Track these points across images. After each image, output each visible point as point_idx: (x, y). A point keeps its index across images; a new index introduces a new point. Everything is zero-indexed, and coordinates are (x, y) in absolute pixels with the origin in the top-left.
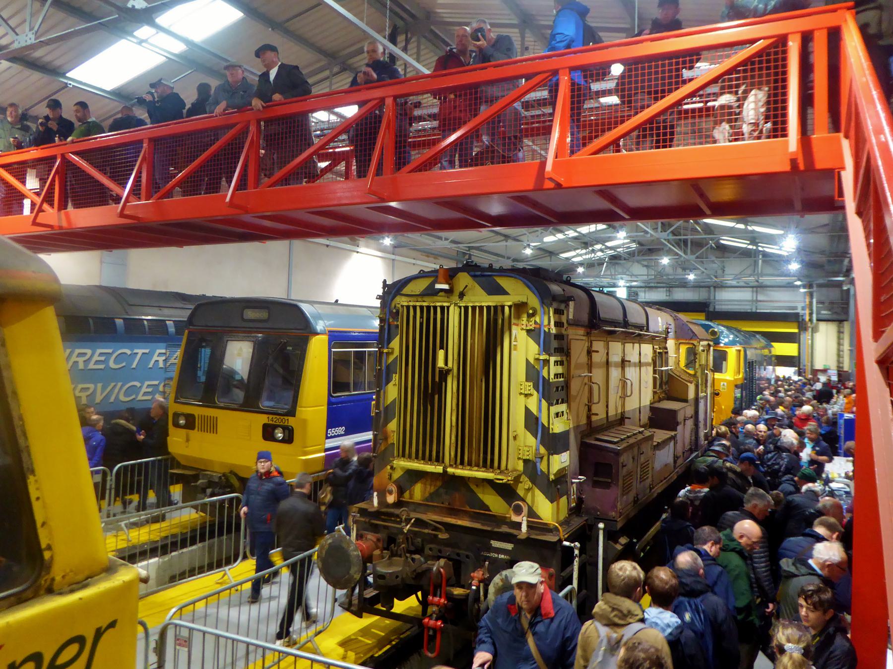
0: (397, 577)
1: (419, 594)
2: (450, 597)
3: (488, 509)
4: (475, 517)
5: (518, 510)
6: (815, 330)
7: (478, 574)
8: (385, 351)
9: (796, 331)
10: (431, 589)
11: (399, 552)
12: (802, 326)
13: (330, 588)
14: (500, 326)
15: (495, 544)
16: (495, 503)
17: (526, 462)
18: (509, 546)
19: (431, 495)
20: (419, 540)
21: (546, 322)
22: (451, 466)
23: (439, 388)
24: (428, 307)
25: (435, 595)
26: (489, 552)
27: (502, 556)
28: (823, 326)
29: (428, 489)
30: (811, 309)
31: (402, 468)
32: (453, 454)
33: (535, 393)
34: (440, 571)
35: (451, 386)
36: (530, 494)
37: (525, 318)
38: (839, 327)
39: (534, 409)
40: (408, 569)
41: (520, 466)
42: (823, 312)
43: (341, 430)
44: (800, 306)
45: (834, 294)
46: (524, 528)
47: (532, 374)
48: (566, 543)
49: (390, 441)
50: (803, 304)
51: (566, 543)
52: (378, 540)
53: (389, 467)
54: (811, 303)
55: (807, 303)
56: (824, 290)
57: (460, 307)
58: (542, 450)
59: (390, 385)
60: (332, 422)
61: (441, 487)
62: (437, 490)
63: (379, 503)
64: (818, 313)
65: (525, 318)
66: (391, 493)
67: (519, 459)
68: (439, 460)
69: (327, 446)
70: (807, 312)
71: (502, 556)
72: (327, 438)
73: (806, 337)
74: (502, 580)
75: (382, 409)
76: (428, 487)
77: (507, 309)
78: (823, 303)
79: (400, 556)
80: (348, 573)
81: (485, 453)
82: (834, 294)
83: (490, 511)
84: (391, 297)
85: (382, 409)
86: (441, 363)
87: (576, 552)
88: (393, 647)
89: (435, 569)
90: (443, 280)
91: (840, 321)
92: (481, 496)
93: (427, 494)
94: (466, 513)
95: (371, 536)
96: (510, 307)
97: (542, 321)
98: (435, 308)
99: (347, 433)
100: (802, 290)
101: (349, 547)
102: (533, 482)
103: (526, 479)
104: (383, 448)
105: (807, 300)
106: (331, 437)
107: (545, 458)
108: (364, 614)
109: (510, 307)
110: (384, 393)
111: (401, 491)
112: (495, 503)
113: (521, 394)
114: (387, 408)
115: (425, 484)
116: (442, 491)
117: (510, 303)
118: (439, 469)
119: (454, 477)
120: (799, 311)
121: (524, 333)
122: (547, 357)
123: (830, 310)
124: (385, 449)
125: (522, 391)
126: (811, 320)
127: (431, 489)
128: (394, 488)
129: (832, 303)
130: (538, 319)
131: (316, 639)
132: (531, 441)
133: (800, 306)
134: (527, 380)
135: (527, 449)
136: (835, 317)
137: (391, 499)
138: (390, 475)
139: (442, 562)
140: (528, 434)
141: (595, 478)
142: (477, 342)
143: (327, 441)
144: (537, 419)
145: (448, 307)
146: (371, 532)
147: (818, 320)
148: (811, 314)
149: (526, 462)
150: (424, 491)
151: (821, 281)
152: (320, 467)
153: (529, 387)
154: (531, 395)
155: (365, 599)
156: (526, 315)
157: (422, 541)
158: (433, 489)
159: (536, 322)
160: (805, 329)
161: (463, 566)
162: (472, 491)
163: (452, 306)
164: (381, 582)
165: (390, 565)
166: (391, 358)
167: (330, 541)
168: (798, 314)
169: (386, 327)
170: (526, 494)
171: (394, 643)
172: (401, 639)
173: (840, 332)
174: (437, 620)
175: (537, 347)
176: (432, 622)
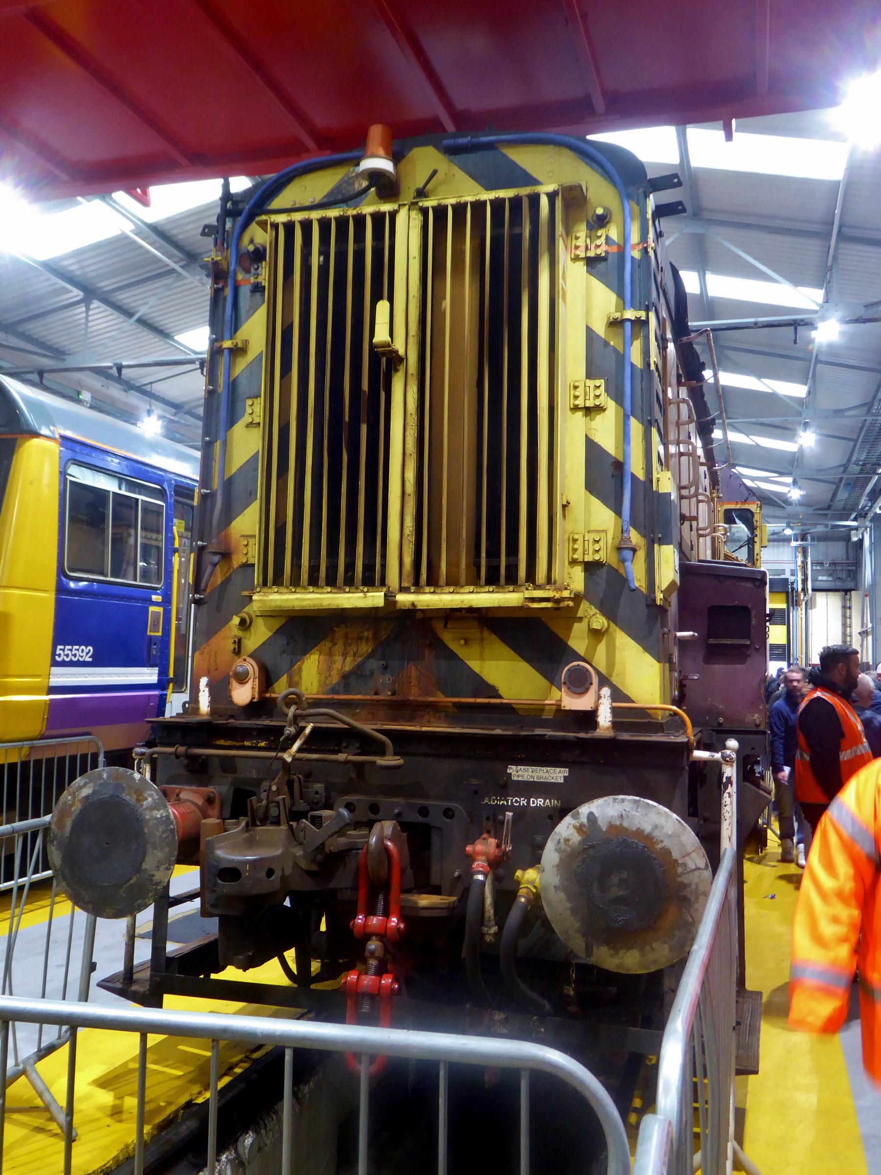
0: (270, 873)
1: (290, 955)
2: (409, 916)
3: (493, 692)
4: (464, 712)
5: (579, 683)
6: (810, 605)
7: (485, 847)
8: (227, 344)
9: (784, 606)
10: (362, 896)
11: (274, 812)
12: (792, 598)
13: (82, 916)
14: (526, 244)
15: (520, 773)
16: (509, 676)
17: (591, 568)
18: (557, 775)
19: (345, 677)
20: (319, 787)
21: (635, 237)
22: (403, 590)
23: (374, 408)
24: (342, 222)
25: (370, 911)
26: (505, 796)
27: (540, 802)
28: (821, 598)
29: (338, 665)
30: (805, 574)
31: (271, 614)
32: (408, 560)
33: (611, 405)
34: (386, 849)
35: (402, 397)
36: (602, 648)
37: (581, 231)
38: (844, 600)
39: (608, 443)
40: (299, 852)
41: (577, 580)
42: (820, 578)
43: (85, 652)
44: (788, 568)
45: (837, 551)
46: (605, 718)
47: (601, 360)
48: (700, 754)
49: (238, 560)
50: (793, 566)
51: (700, 754)
52: (210, 801)
53: (236, 620)
54: (804, 563)
55: (799, 563)
56: (822, 545)
57: (424, 212)
58: (635, 537)
59: (239, 428)
60: (65, 633)
61: (370, 656)
62: (360, 666)
63: (212, 703)
64: (814, 580)
65: (581, 231)
66: (242, 679)
67: (573, 562)
68: (372, 578)
69: (55, 681)
70: (800, 577)
71: (540, 802)
72: (55, 664)
73: (797, 615)
74: (580, 829)
75: (216, 484)
76: (338, 659)
77: (544, 201)
78: (821, 564)
79: (277, 822)
80: (139, 870)
81: (493, 553)
82: (837, 551)
83: (500, 697)
84: (240, 220)
85: (216, 484)
86: (381, 335)
87: (730, 771)
88: (238, 1079)
89: (373, 840)
90: (381, 152)
91: (847, 591)
92: (475, 665)
93: (335, 679)
94: (434, 708)
95: (191, 795)
96: (552, 196)
97: (625, 236)
98: (360, 220)
99: (98, 661)
100: (794, 544)
101: (140, 799)
102: (611, 615)
103: (593, 610)
104: (219, 579)
105: (800, 559)
106: (63, 664)
107: (641, 555)
108: (167, 998)
109: (552, 196)
110: (225, 444)
111: (267, 679)
112: (509, 676)
113: (575, 408)
114: (228, 484)
115: (330, 654)
116: (374, 664)
117: (550, 188)
118: (375, 598)
119: (412, 612)
120: (787, 575)
121: (581, 267)
122: (642, 314)
123: (830, 575)
124: (227, 581)
125: (580, 402)
126: (804, 590)
127: (343, 664)
128: (251, 667)
129: (833, 564)
130: (613, 232)
131: (41, 1066)
132: (603, 517)
133: (788, 568)
134: (589, 376)
135: (590, 537)
136: (839, 585)
137: (243, 694)
138: (239, 642)
139: (388, 827)
140: (596, 503)
141: (711, 641)
142: (461, 300)
143: (55, 670)
144: (619, 466)
145: (393, 215)
146: (190, 783)
147: (813, 590)
148: (804, 581)
149: (591, 568)
150: (325, 672)
151: (820, 529)
152: (36, 726)
153: (596, 391)
154: (600, 409)
155: (170, 960)
156: (583, 227)
157: (327, 789)
158: (349, 664)
159: (608, 240)
160: (797, 604)
161: (435, 839)
162: (453, 656)
163: (403, 212)
164: (225, 887)
165: (251, 843)
166: (242, 365)
167: (86, 792)
168: (787, 580)
169: (228, 292)
170: (592, 649)
171: (238, 1070)
172: (255, 1061)
173: (846, 608)
174: (381, 972)
175: (613, 297)
176: (368, 980)
